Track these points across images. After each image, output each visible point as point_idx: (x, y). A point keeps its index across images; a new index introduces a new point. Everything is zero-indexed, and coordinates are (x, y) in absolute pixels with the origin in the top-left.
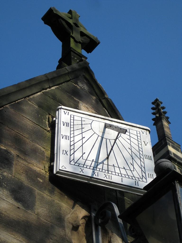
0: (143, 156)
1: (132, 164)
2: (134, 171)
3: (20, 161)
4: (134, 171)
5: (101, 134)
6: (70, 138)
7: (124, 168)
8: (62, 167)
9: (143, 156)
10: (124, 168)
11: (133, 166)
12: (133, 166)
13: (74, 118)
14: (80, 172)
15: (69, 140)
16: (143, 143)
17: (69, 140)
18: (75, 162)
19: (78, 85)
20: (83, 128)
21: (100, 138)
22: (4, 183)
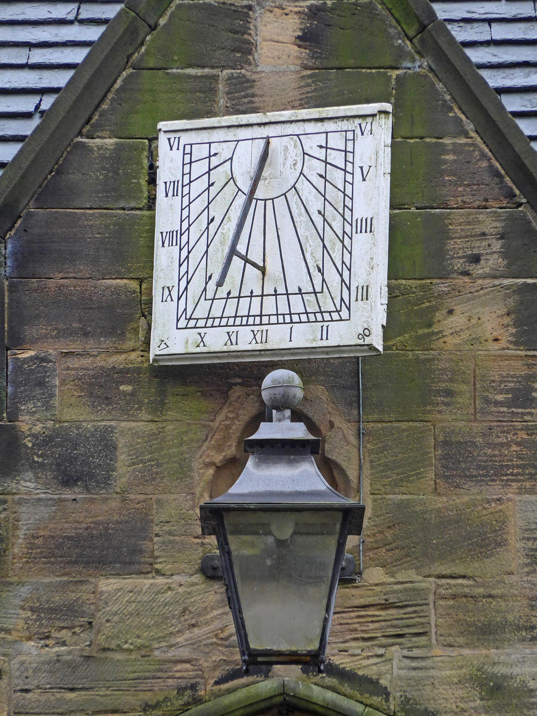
0: (351, 225)
1: (319, 270)
2: (322, 292)
3: (72, 366)
4: (322, 292)
5: (246, 189)
6: (183, 186)
7: (210, 185)
8: (159, 347)
9: (351, 225)
10: (210, 185)
11: (323, 275)
12: (323, 275)
13: (254, 316)
14: (198, 346)
15: (177, 245)
16: (358, 172)
17: (177, 245)
18: (188, 317)
19: (139, 563)
20: (275, 291)
21: (241, 200)
22: (38, 456)
